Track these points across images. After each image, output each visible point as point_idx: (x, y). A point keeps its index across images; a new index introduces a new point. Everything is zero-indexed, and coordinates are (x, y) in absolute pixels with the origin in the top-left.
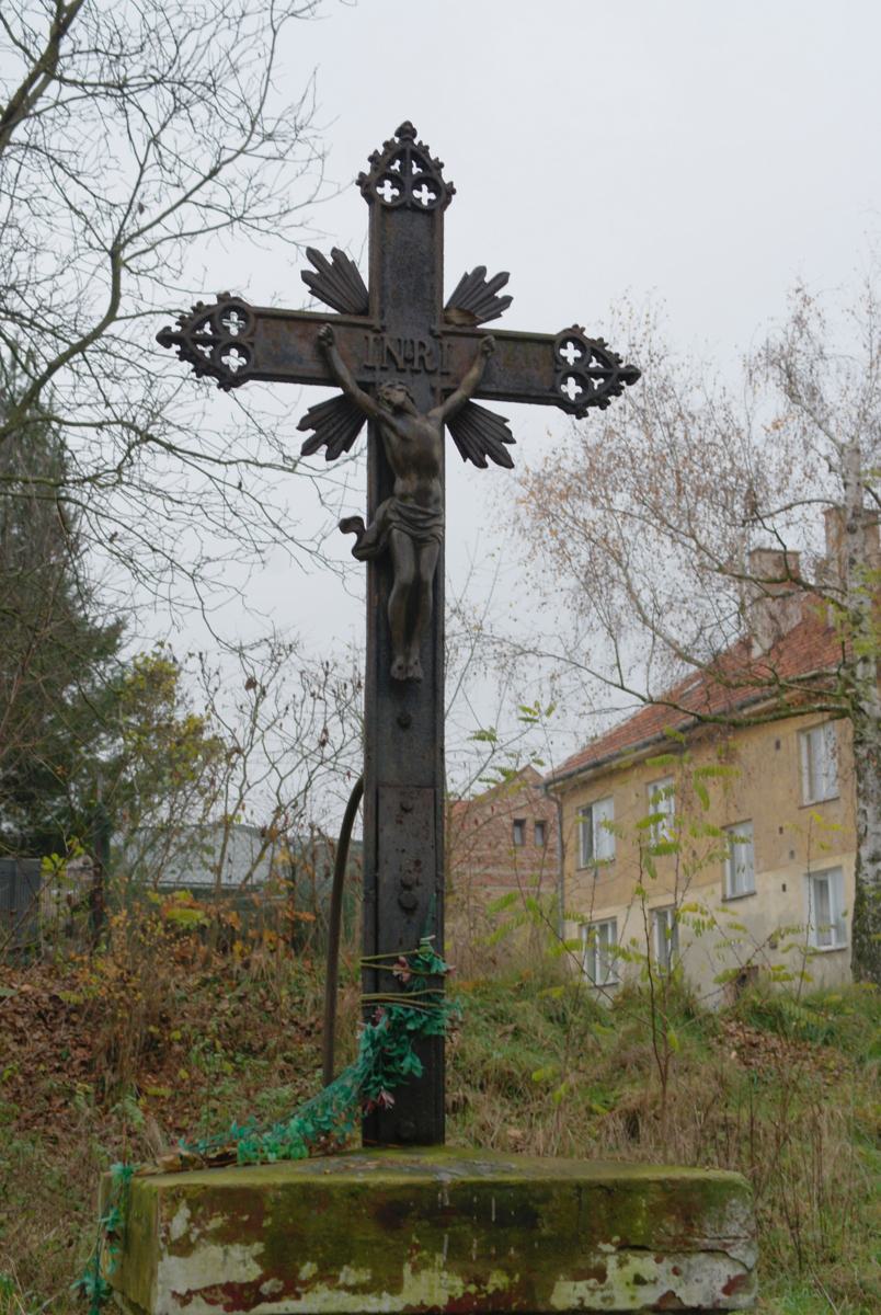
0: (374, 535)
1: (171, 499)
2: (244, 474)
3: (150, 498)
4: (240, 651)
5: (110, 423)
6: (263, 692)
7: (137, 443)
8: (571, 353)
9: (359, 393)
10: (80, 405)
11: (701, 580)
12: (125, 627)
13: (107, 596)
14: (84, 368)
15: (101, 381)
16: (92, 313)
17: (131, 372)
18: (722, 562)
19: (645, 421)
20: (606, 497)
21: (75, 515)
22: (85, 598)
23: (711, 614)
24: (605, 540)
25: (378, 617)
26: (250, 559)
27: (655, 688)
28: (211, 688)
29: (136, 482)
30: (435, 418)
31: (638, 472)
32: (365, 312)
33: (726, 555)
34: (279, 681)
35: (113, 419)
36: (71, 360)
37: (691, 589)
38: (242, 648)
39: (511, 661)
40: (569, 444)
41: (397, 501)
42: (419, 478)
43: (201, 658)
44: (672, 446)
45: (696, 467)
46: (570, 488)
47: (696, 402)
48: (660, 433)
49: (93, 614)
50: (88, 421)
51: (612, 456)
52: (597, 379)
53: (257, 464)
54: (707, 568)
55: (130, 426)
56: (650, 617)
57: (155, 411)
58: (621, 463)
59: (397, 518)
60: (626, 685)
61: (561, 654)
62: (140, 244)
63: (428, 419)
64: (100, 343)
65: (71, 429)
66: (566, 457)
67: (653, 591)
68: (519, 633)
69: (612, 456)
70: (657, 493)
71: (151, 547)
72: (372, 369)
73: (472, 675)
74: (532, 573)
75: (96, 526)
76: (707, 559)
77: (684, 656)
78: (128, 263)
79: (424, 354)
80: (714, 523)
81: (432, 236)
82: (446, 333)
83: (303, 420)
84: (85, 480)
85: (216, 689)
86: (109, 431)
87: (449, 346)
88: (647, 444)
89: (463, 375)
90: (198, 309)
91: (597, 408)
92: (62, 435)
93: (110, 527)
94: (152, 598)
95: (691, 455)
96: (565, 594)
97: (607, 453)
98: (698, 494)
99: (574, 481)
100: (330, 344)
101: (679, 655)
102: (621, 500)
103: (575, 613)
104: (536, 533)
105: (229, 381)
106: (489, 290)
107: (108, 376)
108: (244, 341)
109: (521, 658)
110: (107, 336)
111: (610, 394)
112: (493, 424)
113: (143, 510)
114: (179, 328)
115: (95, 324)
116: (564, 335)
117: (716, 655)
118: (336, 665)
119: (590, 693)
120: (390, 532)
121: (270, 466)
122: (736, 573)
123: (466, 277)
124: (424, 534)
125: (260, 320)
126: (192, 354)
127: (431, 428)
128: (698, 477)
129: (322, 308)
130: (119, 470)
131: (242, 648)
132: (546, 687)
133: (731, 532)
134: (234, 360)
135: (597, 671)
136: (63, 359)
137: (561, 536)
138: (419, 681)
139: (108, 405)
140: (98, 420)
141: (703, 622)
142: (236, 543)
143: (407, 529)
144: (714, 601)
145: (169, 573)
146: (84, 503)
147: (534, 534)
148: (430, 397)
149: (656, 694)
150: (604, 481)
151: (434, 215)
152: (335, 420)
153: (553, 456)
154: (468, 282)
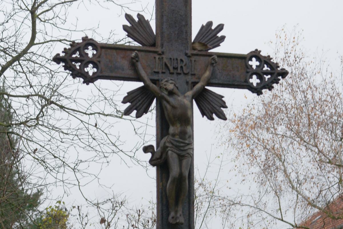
0: (160, 154)
1: (63, 132)
2: (98, 120)
3: (53, 132)
4: (97, 205)
5: (32, 95)
6: (109, 225)
7: (46, 105)
8: (254, 63)
9: (152, 85)
10: (18, 87)
11: (320, 168)
12: (42, 194)
13: (33, 180)
14: (19, 69)
15: (28, 75)
16: (22, 42)
17: (42, 70)
18: (330, 159)
19: (292, 90)
20: (274, 127)
21: (17, 140)
22: (22, 180)
23: (326, 184)
24: (273, 149)
25: (162, 193)
26: (101, 161)
27: (298, 220)
28: (84, 223)
29: (46, 124)
30: (188, 96)
31: (289, 115)
32: (154, 45)
33: (332, 155)
34: (116, 219)
35: (33, 93)
36: (13, 65)
37: (315, 172)
38: (98, 204)
39: (228, 208)
40: (255, 102)
41: (170, 137)
42: (181, 126)
43: (78, 209)
44: (306, 102)
45: (318, 112)
46: (256, 123)
47: (317, 80)
48: (300, 96)
49: (26, 188)
50: (22, 95)
51: (276, 107)
52: (267, 75)
53: (104, 115)
54: (323, 162)
55: (42, 97)
56: (296, 186)
57: (54, 89)
58: (281, 111)
59: (170, 145)
60: (284, 219)
61: (252, 204)
62: (45, 7)
63: (185, 97)
64: (27, 56)
65: (13, 98)
66: (254, 108)
67: (297, 173)
68: (232, 195)
69: (276, 107)
70: (299, 125)
71: (54, 155)
72: (158, 73)
73: (209, 215)
74: (238, 166)
75: (26, 145)
76: (323, 157)
77: (312, 204)
78: (40, 17)
79: (183, 65)
80: (326, 140)
81: (186, 7)
82: (193, 55)
83: (125, 98)
84: (21, 123)
85: (86, 224)
86: (32, 99)
87: (195, 61)
88: (293, 102)
89: (202, 75)
91: (267, 90)
92: (9, 101)
93: (33, 146)
94: (54, 180)
95: (315, 106)
96: (254, 175)
97: (273, 106)
98: (318, 125)
99: (258, 120)
100: (137, 61)
101: (310, 204)
102: (281, 129)
103: (259, 184)
104: (240, 146)
105: (88, 80)
106: (214, 33)
107: (30, 72)
108: (95, 61)
109: (233, 206)
110: (30, 53)
111: (274, 83)
112: (217, 99)
113: (49, 138)
114: (63, 54)
115: (24, 47)
116: (251, 55)
117: (328, 205)
118: (143, 211)
119: (267, 223)
120: (167, 153)
121: (110, 115)
122: (338, 164)
123: (203, 27)
124: (183, 153)
125: (103, 50)
126: (70, 67)
127: (186, 102)
128: (319, 117)
129: (136, 44)
130: (37, 119)
131: (98, 204)
132: (245, 220)
133: (335, 144)
134: (90, 70)
135: (270, 212)
136: (9, 64)
137: (251, 147)
138: (182, 224)
139: (31, 86)
140: (26, 94)
141: (321, 188)
142: (94, 153)
143: (175, 151)
144: (327, 178)
145: (62, 168)
146: (21, 134)
147: (238, 146)
148: (186, 86)
149: (298, 223)
150: (273, 120)
152: (140, 98)
153: (247, 108)
154: (204, 29)
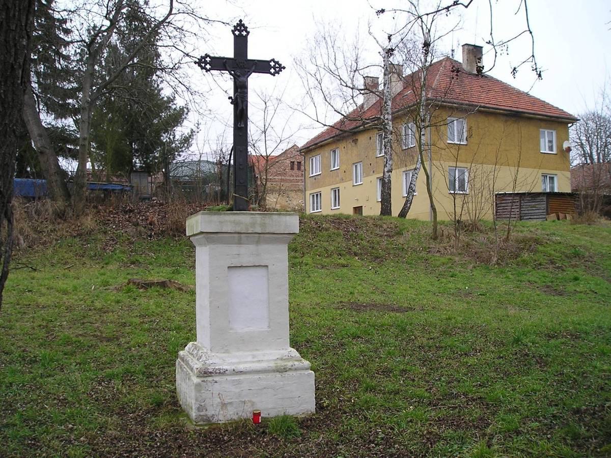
90: (201, 57)
151: (246, 37)
